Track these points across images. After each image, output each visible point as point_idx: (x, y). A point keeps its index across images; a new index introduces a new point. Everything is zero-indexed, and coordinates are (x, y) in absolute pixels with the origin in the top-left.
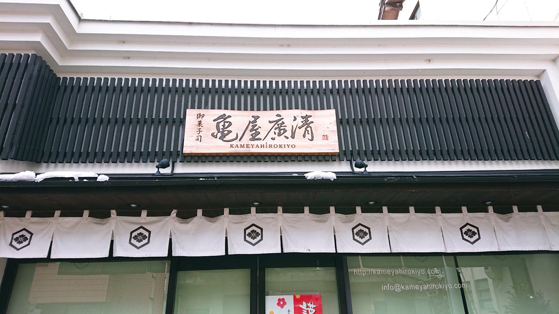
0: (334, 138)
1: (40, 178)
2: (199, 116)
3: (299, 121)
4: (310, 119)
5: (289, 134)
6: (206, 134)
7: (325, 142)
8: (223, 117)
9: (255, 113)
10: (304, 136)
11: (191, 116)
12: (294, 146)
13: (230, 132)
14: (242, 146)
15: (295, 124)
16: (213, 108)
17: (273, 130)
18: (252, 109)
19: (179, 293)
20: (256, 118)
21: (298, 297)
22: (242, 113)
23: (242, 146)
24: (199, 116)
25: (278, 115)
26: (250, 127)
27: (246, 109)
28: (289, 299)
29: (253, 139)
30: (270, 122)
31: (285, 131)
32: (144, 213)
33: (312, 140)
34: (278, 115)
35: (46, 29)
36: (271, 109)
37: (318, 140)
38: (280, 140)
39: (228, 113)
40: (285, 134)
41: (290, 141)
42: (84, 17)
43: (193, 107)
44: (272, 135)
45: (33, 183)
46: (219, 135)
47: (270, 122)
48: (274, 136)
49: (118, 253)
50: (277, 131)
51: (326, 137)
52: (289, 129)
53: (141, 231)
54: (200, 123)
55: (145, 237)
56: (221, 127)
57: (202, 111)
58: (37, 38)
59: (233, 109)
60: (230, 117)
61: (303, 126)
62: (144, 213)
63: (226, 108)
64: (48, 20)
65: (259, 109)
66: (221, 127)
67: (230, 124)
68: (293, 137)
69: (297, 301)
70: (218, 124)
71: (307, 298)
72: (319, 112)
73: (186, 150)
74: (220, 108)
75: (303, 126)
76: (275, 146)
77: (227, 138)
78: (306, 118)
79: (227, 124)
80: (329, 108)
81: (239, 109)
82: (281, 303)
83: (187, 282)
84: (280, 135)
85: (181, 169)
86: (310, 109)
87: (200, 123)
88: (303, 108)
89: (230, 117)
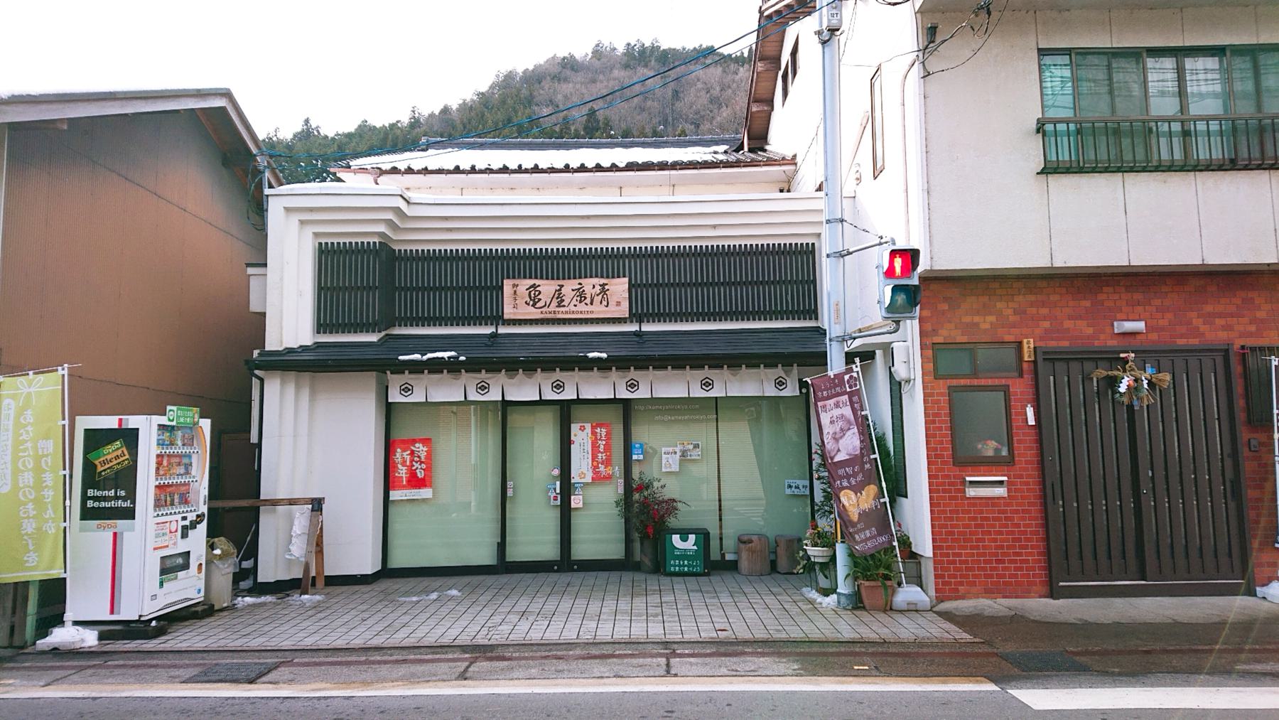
0: (626, 305)
1: (425, 358)
2: (514, 286)
3: (598, 288)
4: (606, 287)
5: (588, 301)
6: (520, 302)
7: (618, 308)
8: (534, 286)
9: (561, 282)
10: (601, 303)
11: (508, 285)
12: (592, 312)
13: (540, 300)
14: (550, 313)
15: (593, 291)
16: (525, 277)
17: (575, 298)
18: (558, 279)
19: (393, 423)
20: (562, 286)
21: (594, 424)
22: (553, 282)
23: (550, 313)
24: (514, 286)
25: (580, 284)
26: (556, 296)
27: (553, 279)
28: (588, 427)
29: (559, 306)
30: (573, 290)
31: (585, 298)
32: (483, 371)
33: (607, 306)
34: (580, 284)
35: (389, 222)
36: (575, 278)
37: (612, 307)
38: (582, 307)
39: (537, 282)
40: (586, 301)
41: (590, 308)
42: (413, 201)
43: (508, 278)
44: (574, 302)
45: (422, 361)
46: (531, 303)
47: (573, 290)
48: (576, 303)
49: (471, 398)
50: (579, 299)
51: (618, 304)
52: (588, 296)
53: (483, 384)
54: (515, 292)
55: (486, 388)
56: (533, 296)
57: (516, 282)
58: (381, 228)
59: (542, 278)
60: (539, 286)
61: (600, 293)
62: (483, 371)
63: (536, 278)
64: (390, 216)
65: (564, 279)
66: (533, 296)
67: (540, 293)
68: (592, 304)
69: (593, 428)
70: (530, 292)
71: (601, 425)
72: (617, 280)
73: (506, 317)
74: (530, 278)
75: (600, 293)
76: (578, 312)
77: (538, 305)
78: (603, 285)
79: (537, 293)
80: (624, 276)
81: (547, 279)
82: (582, 428)
83: (490, 437)
84: (581, 302)
85: (502, 330)
86: (608, 277)
87: (515, 292)
88: (602, 277)
89: (539, 286)
